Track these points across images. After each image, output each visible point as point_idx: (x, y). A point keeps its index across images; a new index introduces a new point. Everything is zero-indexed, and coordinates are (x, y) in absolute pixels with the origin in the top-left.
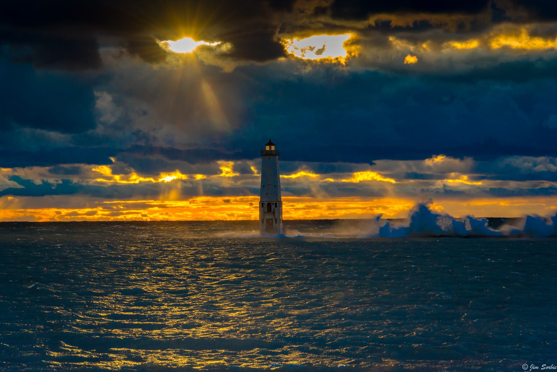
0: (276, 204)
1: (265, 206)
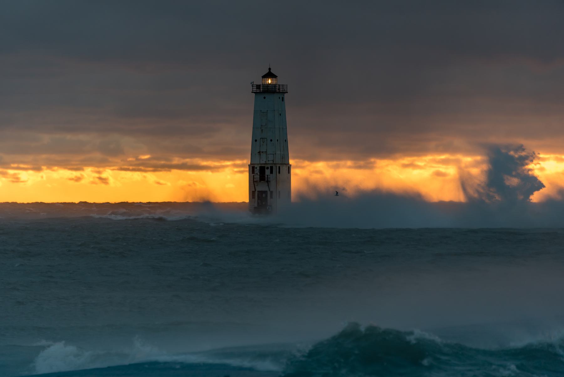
0: (272, 168)
1: (257, 171)
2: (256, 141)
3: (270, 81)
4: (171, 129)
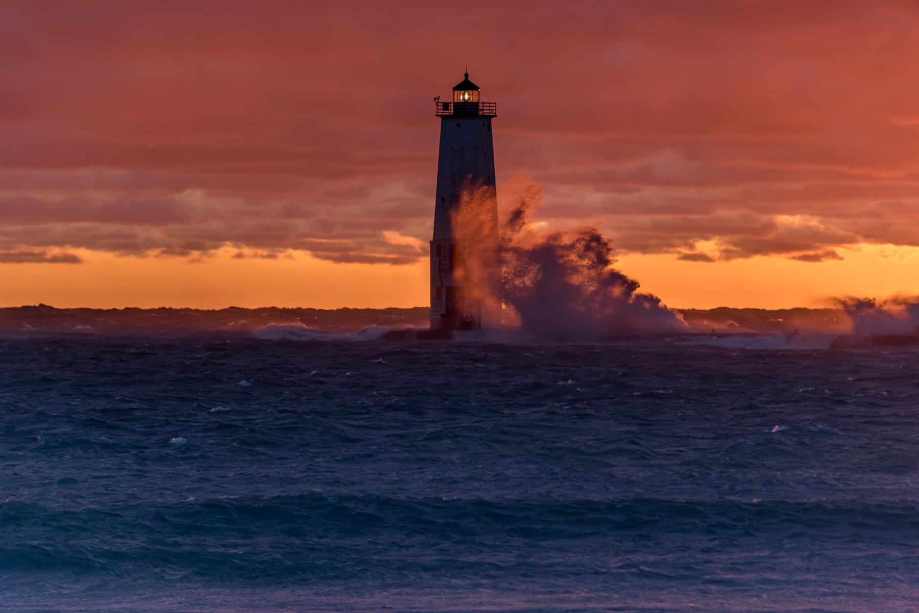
2: (443, 199)
3: (467, 97)
4: (275, 165)
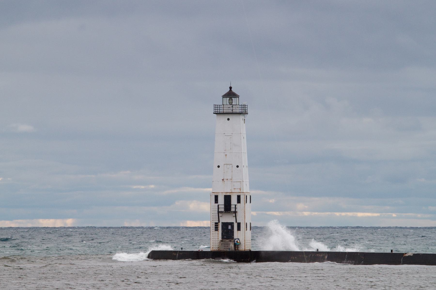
1: (221, 201)
